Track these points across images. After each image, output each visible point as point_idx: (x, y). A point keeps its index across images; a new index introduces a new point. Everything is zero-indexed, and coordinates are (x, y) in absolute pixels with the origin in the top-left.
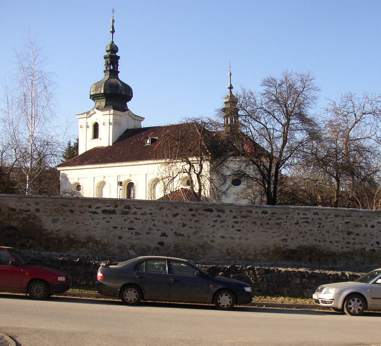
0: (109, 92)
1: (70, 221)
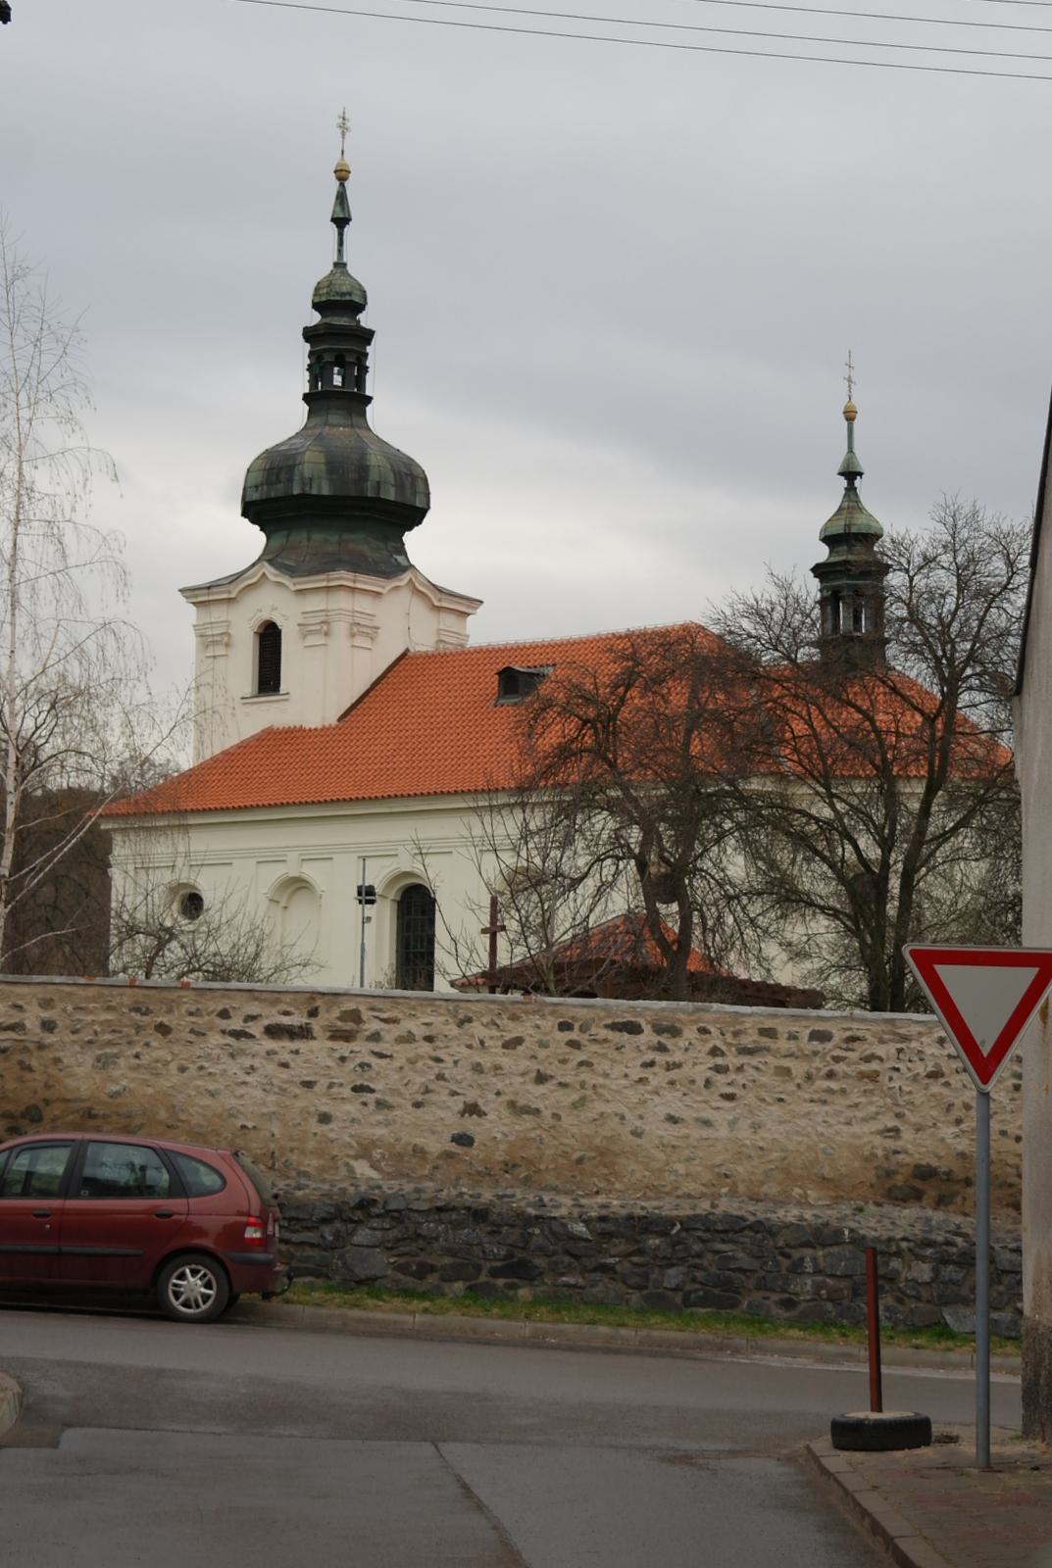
0: (325, 491)
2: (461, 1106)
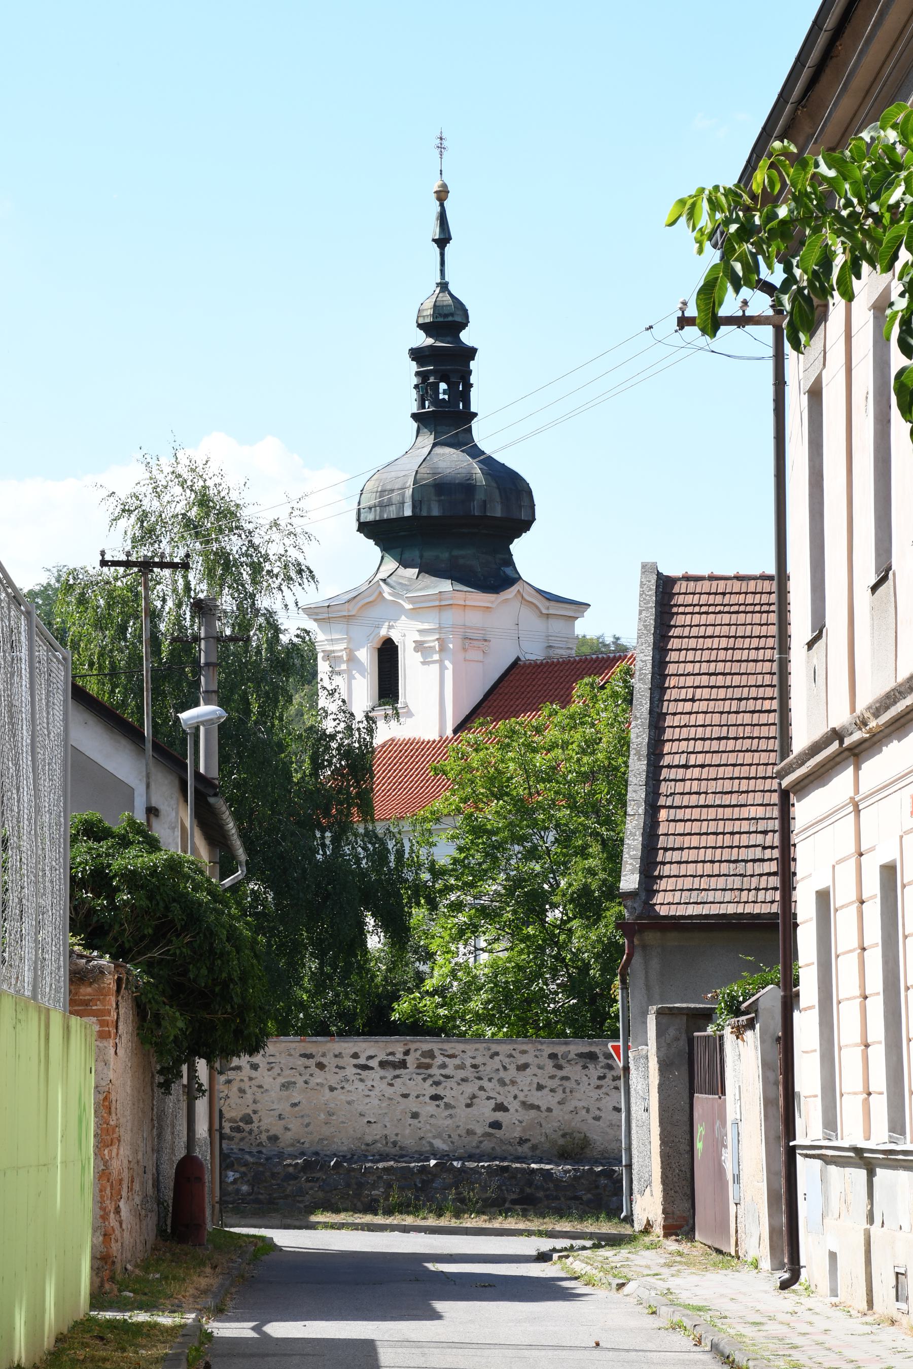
0: (435, 512)
1: (318, 1084)
2: (493, 1106)
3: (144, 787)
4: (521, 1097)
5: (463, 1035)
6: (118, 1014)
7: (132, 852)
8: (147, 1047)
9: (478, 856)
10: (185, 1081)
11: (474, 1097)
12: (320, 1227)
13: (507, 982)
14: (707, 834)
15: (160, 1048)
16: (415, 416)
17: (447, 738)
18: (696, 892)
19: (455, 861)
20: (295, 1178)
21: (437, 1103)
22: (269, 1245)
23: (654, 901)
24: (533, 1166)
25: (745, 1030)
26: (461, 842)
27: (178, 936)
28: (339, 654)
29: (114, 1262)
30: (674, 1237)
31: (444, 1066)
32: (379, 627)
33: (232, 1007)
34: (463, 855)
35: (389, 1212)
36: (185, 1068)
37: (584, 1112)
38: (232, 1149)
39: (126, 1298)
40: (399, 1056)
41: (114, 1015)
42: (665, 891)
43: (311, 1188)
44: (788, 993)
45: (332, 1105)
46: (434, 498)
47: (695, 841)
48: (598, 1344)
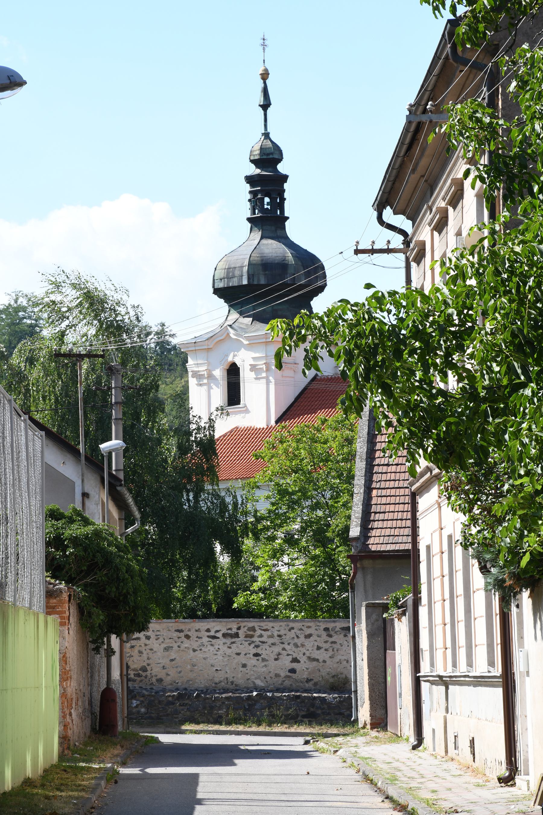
1: (186, 648)
2: (291, 659)
3: (81, 481)
4: (308, 654)
5: (277, 617)
6: (69, 613)
7: (74, 526)
8: (84, 629)
9: (284, 507)
10: (105, 647)
11: (279, 654)
12: (188, 733)
13: (303, 584)
14: (399, 504)
15: (91, 629)
16: (249, 220)
17: (272, 426)
18: (392, 537)
19: (270, 511)
20: (173, 703)
21: (257, 658)
22: (157, 740)
23: (368, 542)
24: (315, 695)
25: (402, 616)
26: (273, 500)
27: (100, 570)
28: (202, 373)
29: (69, 740)
30: (376, 730)
31: (261, 636)
32: (227, 356)
33: (129, 607)
34: (275, 507)
35: (229, 723)
36: (105, 639)
37: (345, 662)
38: (135, 687)
39: (76, 757)
40: (234, 630)
41: (67, 613)
42: (375, 536)
43: (183, 710)
44: (416, 597)
45: (195, 660)
46: (261, 273)
47: (392, 508)
48: (308, 773)
